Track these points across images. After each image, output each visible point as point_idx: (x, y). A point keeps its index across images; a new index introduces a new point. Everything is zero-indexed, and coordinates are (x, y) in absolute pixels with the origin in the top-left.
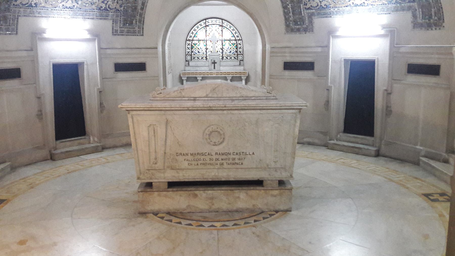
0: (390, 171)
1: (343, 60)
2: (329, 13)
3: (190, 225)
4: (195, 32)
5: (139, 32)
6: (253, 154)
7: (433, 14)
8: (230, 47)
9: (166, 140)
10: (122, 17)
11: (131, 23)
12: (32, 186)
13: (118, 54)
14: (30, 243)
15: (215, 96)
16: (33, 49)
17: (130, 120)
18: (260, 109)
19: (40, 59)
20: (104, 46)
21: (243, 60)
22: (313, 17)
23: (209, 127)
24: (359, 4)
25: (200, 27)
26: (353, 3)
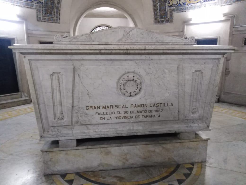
0: (239, 113)
6: (172, 105)
9: (73, 91)
10: (44, 8)
11: (51, 14)
13: (39, 35)
15: (130, 41)
18: (183, 54)
20: (31, 28)
22: (173, 12)
23: (124, 74)
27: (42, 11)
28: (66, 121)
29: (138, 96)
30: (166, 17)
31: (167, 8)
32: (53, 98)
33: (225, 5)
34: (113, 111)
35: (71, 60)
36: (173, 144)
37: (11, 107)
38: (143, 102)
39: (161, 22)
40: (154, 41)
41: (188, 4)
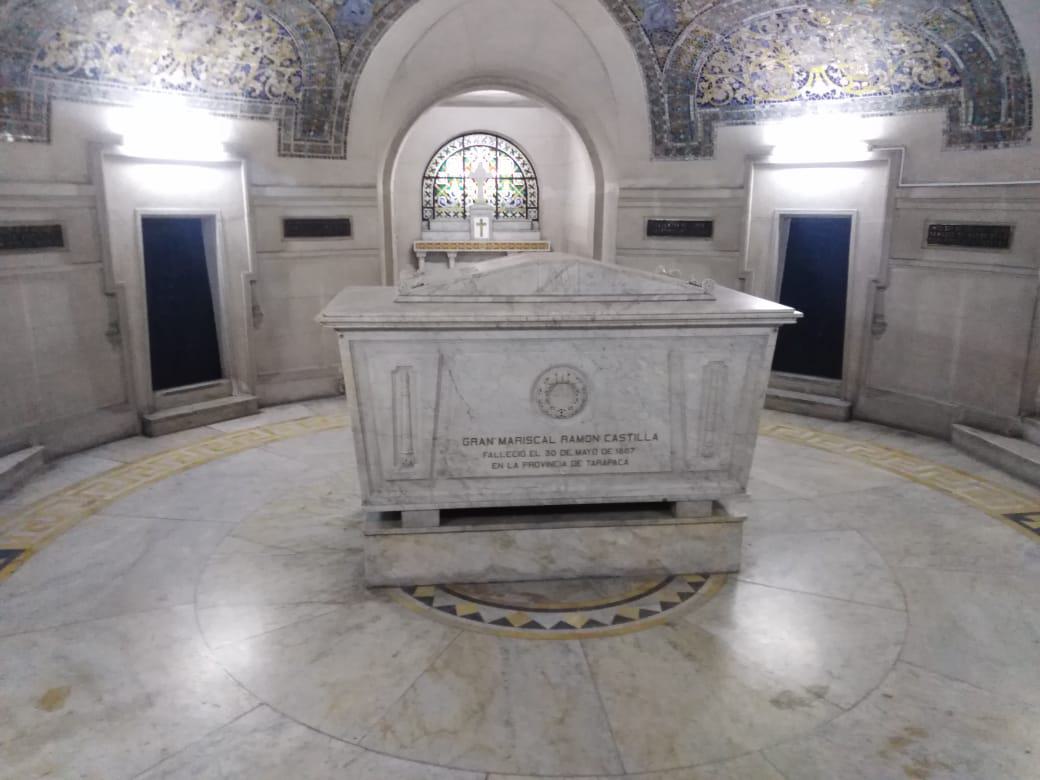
0: (895, 456)
1: (777, 216)
2: (751, 115)
3: (504, 622)
4: (441, 162)
5: (337, 150)
7: (1003, 111)
8: (512, 192)
9: (437, 404)
11: (320, 130)
12: (93, 508)
14: (78, 702)
16: (91, 179)
17: (345, 353)
18: (680, 327)
19: (111, 205)
20: (259, 179)
21: (537, 220)
22: (714, 124)
23: (548, 370)
24: (821, 95)
25: (452, 151)
26: (808, 92)
27: (296, 124)
28: (419, 469)
29: (579, 418)
30: (692, 137)
31: (695, 110)
32: (394, 418)
33: (873, 115)
34: (520, 450)
35: (435, 341)
36: (659, 528)
37: (205, 425)
38: (589, 430)
39: (674, 152)
40: (619, 292)
41: (761, 102)
